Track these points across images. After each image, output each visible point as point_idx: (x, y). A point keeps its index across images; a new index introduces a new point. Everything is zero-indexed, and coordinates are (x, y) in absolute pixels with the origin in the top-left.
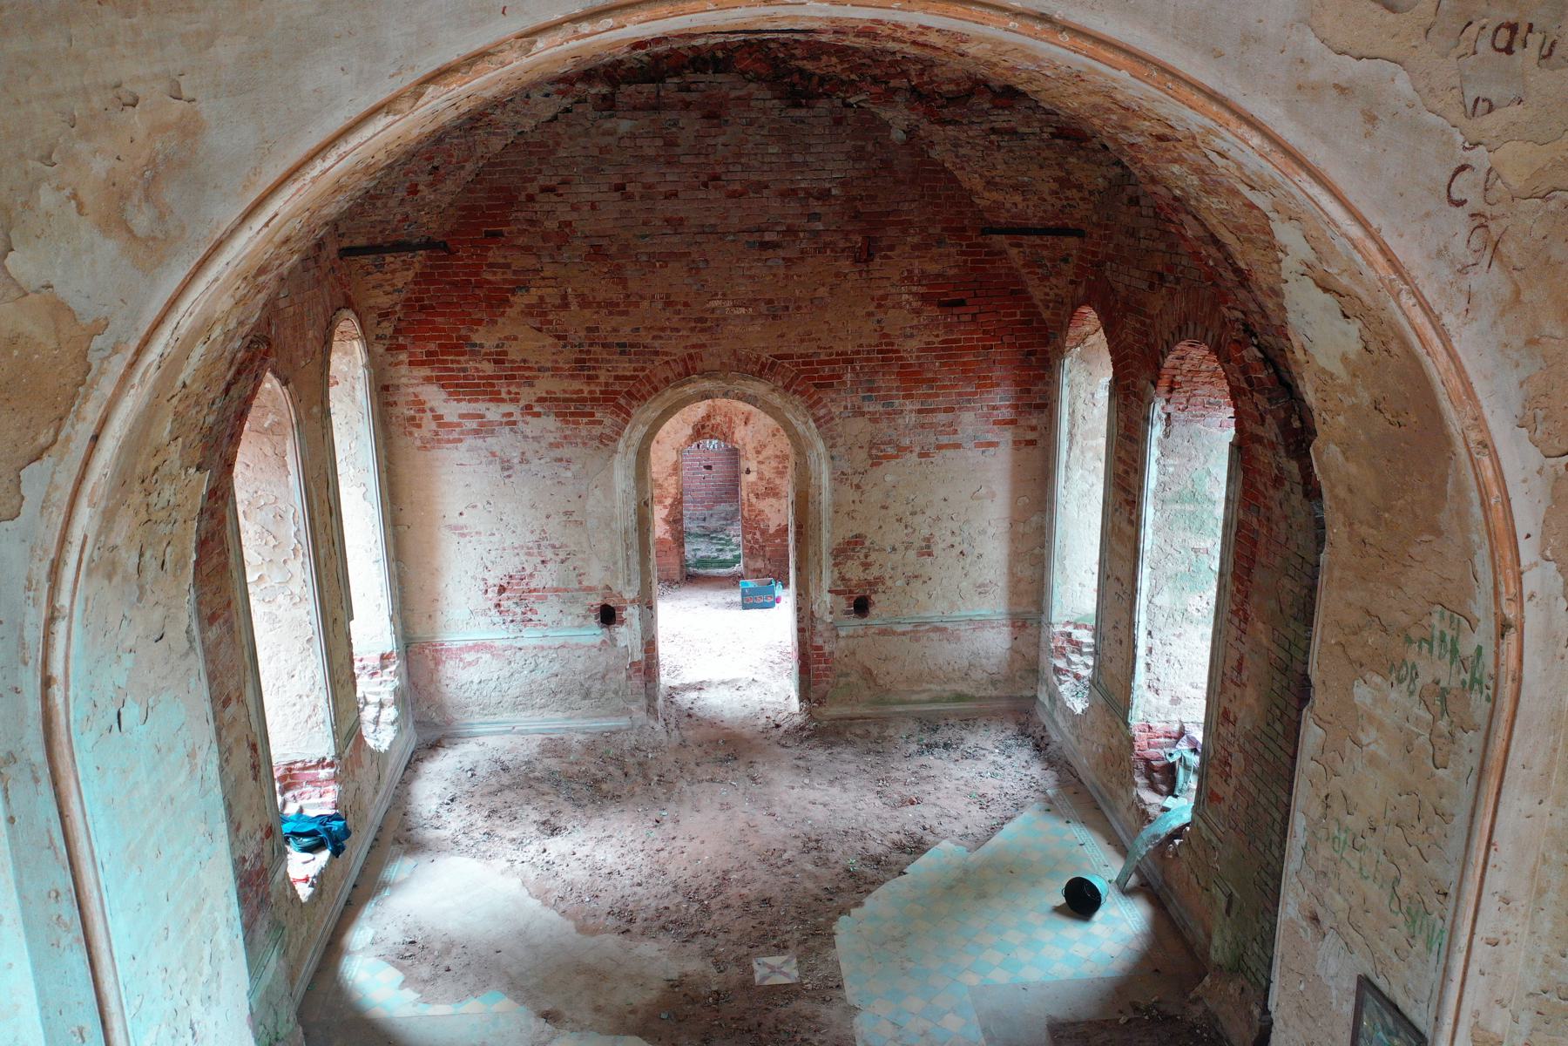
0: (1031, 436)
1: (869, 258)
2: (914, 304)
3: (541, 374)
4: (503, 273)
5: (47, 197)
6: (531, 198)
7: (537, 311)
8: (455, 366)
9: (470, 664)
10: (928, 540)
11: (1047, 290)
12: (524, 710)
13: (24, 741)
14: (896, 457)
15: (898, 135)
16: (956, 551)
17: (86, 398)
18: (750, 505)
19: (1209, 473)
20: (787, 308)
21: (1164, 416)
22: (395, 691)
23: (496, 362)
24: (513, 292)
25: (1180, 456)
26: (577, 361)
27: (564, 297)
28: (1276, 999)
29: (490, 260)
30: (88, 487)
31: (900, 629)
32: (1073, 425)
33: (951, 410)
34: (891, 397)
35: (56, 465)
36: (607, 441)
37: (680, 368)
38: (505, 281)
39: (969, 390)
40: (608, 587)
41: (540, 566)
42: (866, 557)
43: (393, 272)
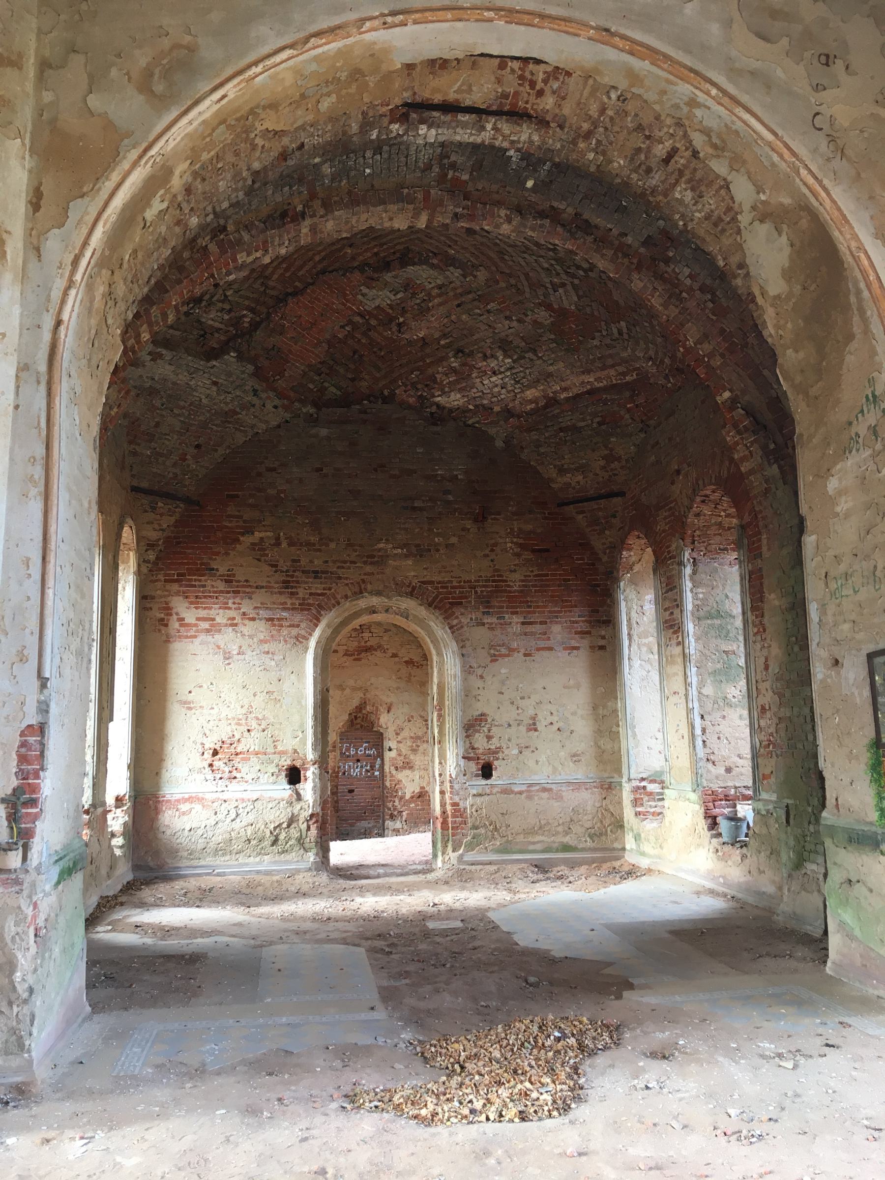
0: (602, 642)
1: (485, 518)
2: (515, 550)
3: (257, 590)
4: (237, 522)
5: (114, 72)
6: (259, 474)
7: (258, 548)
8: (197, 583)
9: (184, 813)
10: (534, 719)
11: (604, 541)
12: (223, 855)
13: (36, 358)
14: (508, 656)
15: (499, 444)
16: (555, 727)
17: (113, 170)
18: (392, 776)
19: (727, 596)
20: (430, 550)
21: (692, 560)
22: (124, 824)
23: (226, 581)
24: (243, 534)
25: (708, 586)
26: (284, 582)
27: (278, 538)
28: (822, 756)
29: (229, 513)
30: (105, 216)
31: (517, 789)
32: (630, 627)
33: (545, 623)
34: (503, 613)
35: (90, 201)
36: (301, 640)
37: (357, 590)
38: (238, 527)
39: (556, 609)
40: (295, 751)
41: (246, 733)
42: (489, 731)
43: (161, 515)
